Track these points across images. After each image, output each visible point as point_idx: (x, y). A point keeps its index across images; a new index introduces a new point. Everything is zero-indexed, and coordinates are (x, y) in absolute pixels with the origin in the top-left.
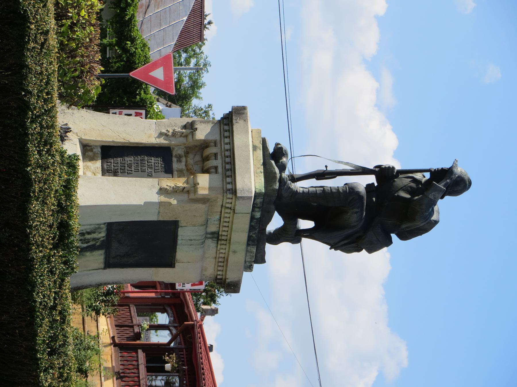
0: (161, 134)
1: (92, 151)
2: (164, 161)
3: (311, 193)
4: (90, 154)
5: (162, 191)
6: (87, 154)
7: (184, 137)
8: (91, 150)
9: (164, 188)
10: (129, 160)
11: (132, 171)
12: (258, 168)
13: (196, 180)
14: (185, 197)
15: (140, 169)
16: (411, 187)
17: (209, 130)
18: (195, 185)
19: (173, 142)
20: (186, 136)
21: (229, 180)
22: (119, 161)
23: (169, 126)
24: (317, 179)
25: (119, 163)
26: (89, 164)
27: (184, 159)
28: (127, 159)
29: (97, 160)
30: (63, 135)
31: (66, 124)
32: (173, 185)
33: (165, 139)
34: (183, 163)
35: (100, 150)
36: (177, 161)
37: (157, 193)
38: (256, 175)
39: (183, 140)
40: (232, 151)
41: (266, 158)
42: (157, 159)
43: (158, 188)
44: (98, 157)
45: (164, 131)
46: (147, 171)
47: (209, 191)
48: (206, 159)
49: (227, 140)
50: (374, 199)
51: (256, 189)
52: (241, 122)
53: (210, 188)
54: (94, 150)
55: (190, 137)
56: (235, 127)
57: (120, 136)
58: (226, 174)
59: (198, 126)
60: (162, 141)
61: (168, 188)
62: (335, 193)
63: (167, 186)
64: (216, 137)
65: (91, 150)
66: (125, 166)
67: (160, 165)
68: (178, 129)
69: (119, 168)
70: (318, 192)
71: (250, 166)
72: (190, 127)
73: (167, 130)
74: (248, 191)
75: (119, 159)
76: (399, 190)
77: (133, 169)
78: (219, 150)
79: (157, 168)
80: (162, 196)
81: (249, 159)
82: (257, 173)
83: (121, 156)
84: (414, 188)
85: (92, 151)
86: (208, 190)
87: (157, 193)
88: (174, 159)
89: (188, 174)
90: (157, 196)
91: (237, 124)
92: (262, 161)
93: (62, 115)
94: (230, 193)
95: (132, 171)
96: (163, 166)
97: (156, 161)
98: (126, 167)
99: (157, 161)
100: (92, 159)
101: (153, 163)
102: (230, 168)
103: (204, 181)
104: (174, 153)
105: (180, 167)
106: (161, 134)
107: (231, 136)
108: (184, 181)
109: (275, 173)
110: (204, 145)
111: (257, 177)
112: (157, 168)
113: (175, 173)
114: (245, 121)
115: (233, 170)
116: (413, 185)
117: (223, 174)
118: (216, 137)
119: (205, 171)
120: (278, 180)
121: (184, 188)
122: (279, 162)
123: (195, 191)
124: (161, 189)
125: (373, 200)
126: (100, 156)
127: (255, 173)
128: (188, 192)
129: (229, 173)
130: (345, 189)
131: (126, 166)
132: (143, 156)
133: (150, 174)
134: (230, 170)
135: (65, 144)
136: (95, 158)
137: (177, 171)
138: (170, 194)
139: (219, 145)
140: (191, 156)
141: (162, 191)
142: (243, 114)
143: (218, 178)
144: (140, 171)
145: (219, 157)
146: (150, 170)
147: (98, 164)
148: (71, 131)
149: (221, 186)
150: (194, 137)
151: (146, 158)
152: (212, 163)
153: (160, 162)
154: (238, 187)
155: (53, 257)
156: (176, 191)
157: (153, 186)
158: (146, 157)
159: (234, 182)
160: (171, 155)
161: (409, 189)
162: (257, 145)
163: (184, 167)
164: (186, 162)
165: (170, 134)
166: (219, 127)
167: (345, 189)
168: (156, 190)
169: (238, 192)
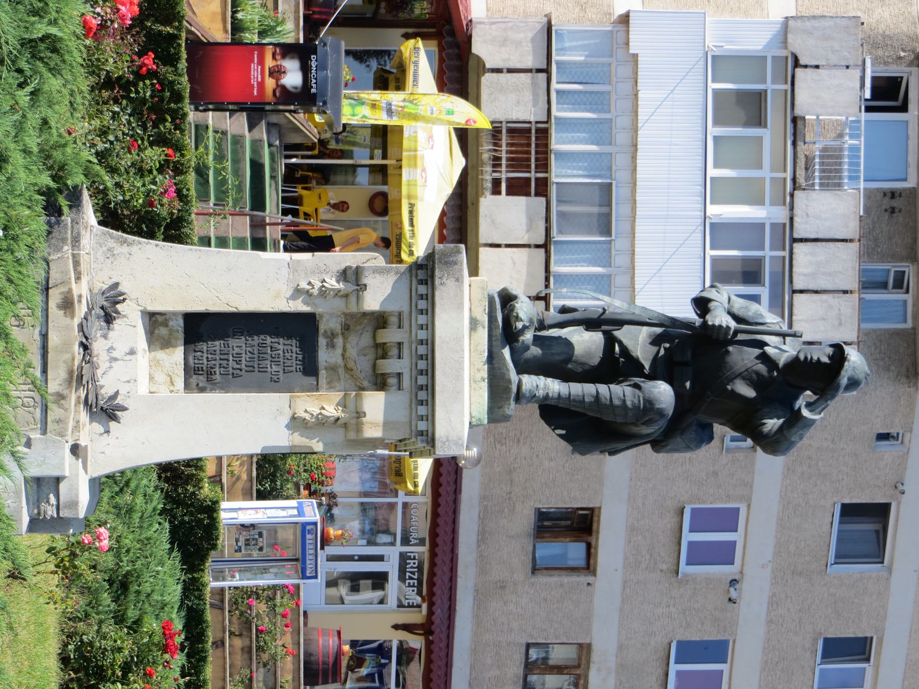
0: (298, 292)
1: (167, 326)
2: (302, 347)
3: (574, 400)
4: (163, 331)
5: (296, 423)
6: (156, 331)
7: (342, 296)
8: (165, 324)
9: (300, 418)
10: (237, 344)
11: (241, 370)
12: (479, 370)
13: (362, 405)
14: (338, 435)
15: (256, 366)
16: (757, 373)
17: (388, 290)
18: (359, 414)
19: (320, 308)
20: (346, 296)
21: (422, 410)
22: (217, 348)
23: (313, 273)
24: (587, 329)
25: (218, 352)
26: (161, 355)
27: (339, 341)
28: (233, 342)
29: (175, 346)
30: (109, 310)
31: (116, 285)
32: (316, 411)
33: (305, 303)
34: (339, 351)
35: (181, 322)
36: (327, 345)
37: (287, 427)
38: (473, 385)
39: (339, 304)
40: (429, 343)
41: (494, 343)
42: (289, 342)
43: (288, 414)
44: (177, 339)
45: (304, 285)
46: (269, 369)
47: (384, 430)
48: (381, 351)
49: (422, 319)
50: (688, 384)
51: (471, 417)
52: (450, 283)
53: (387, 425)
54: (171, 323)
55: (353, 299)
56: (437, 293)
57: (221, 297)
58: (416, 395)
59: (368, 279)
60: (299, 306)
61: (307, 417)
62: (618, 407)
63: (306, 411)
64: (402, 305)
65: (165, 324)
66: (228, 360)
67: (294, 355)
68: (332, 283)
69: (217, 363)
70: (586, 400)
71: (463, 385)
72: (354, 278)
73: (310, 283)
74: (456, 443)
75: (217, 343)
76: (736, 377)
77: (243, 366)
78: (407, 335)
79: (288, 363)
80: (296, 434)
81: (462, 369)
82: (475, 382)
83: (223, 336)
84: (763, 376)
85: (167, 326)
86: (381, 428)
87: (287, 427)
88: (322, 342)
89: (348, 376)
90: (287, 432)
91: (442, 287)
92: (486, 354)
93: (109, 261)
94: (422, 441)
95: (241, 370)
96: (300, 357)
97: (286, 348)
98: (231, 362)
99: (289, 347)
100: (167, 344)
101: (281, 352)
102: (425, 383)
103: (375, 405)
104: (322, 328)
105: (332, 361)
106: (298, 292)
107: (430, 311)
108: (338, 399)
109: (510, 381)
110: (380, 320)
111: (475, 389)
112: (288, 363)
113: (323, 373)
114: (457, 280)
115: (430, 388)
116: (762, 368)
117: (411, 393)
118: (402, 305)
119: (380, 383)
120: (513, 395)
121: (338, 419)
122: (517, 341)
123: (359, 428)
124: (293, 418)
125: (685, 387)
126: (181, 336)
127: (473, 380)
128: (345, 425)
129: (422, 395)
130: (636, 401)
131: (231, 358)
132: (262, 337)
133: (275, 378)
134: (424, 392)
135: (113, 330)
136: (173, 341)
137: (326, 368)
138: (311, 428)
139: (406, 323)
140: (353, 339)
141: (296, 423)
142: (456, 263)
143: (402, 399)
144: (256, 369)
145: (406, 352)
146: (275, 368)
147: (178, 354)
148: (124, 300)
149: (407, 419)
150: (360, 305)
151: (269, 340)
152: (390, 366)
153: (294, 349)
154: (437, 435)
155: (101, 541)
156: (321, 424)
157: (280, 412)
158: (268, 338)
159: (430, 417)
160: (317, 330)
161: (754, 376)
162: (479, 318)
163: (340, 361)
164: (345, 350)
165: (315, 292)
166: (408, 281)
167: (636, 401)
168: (286, 419)
169: (438, 444)
